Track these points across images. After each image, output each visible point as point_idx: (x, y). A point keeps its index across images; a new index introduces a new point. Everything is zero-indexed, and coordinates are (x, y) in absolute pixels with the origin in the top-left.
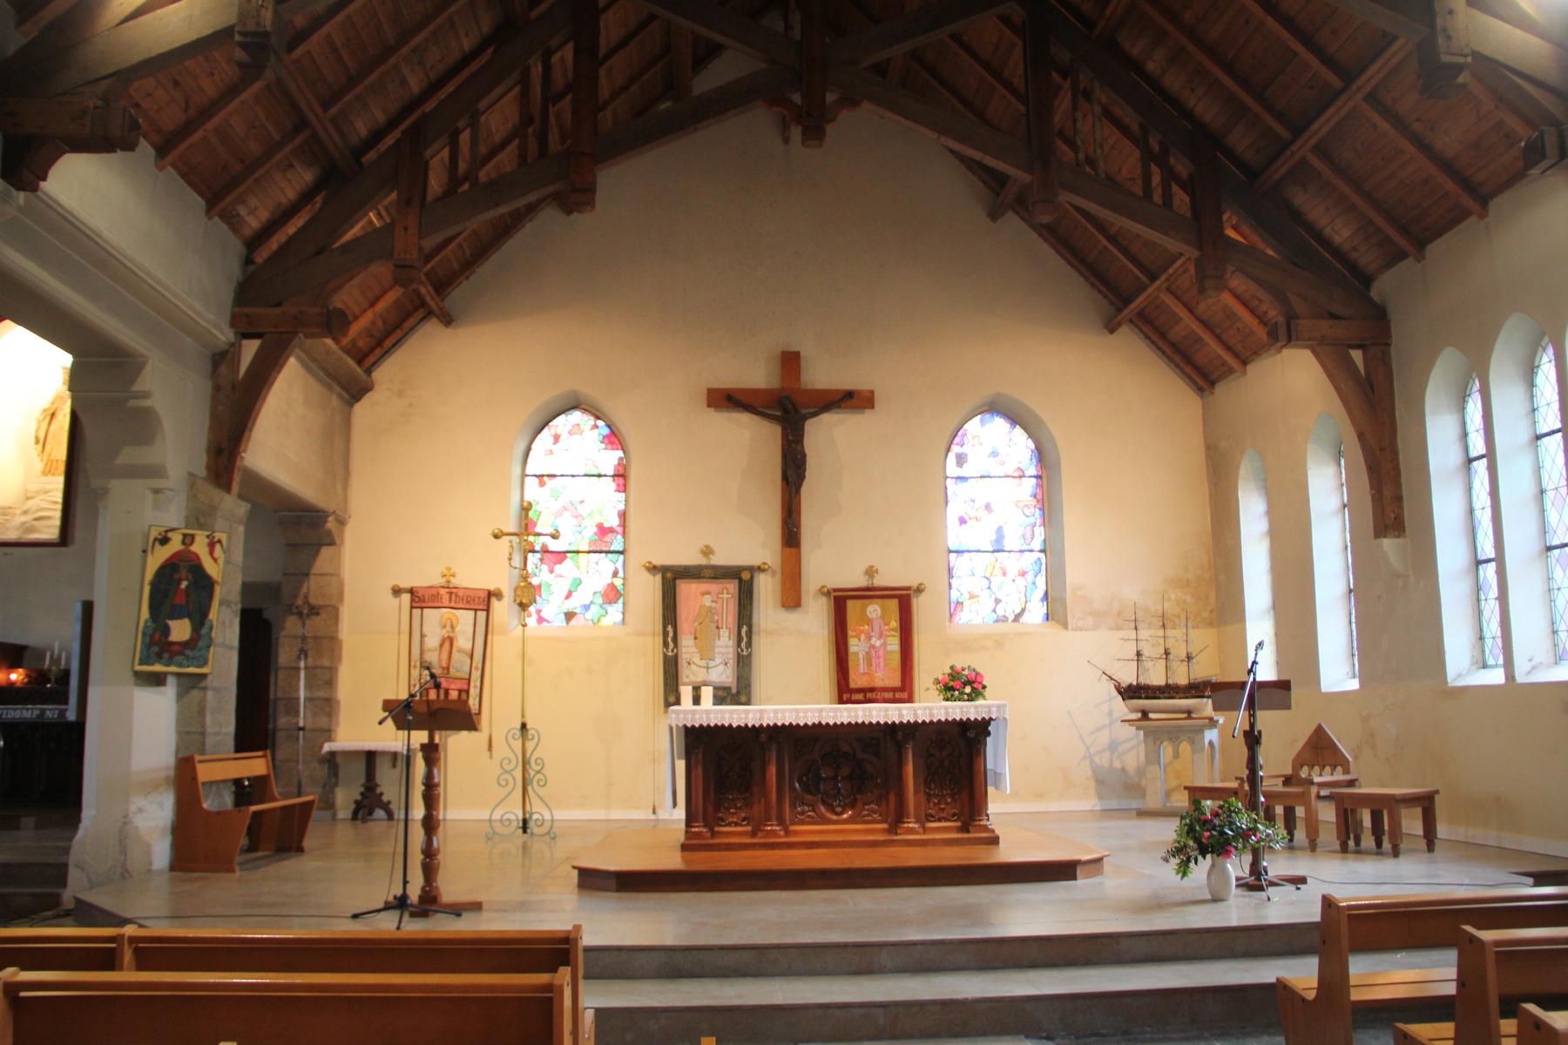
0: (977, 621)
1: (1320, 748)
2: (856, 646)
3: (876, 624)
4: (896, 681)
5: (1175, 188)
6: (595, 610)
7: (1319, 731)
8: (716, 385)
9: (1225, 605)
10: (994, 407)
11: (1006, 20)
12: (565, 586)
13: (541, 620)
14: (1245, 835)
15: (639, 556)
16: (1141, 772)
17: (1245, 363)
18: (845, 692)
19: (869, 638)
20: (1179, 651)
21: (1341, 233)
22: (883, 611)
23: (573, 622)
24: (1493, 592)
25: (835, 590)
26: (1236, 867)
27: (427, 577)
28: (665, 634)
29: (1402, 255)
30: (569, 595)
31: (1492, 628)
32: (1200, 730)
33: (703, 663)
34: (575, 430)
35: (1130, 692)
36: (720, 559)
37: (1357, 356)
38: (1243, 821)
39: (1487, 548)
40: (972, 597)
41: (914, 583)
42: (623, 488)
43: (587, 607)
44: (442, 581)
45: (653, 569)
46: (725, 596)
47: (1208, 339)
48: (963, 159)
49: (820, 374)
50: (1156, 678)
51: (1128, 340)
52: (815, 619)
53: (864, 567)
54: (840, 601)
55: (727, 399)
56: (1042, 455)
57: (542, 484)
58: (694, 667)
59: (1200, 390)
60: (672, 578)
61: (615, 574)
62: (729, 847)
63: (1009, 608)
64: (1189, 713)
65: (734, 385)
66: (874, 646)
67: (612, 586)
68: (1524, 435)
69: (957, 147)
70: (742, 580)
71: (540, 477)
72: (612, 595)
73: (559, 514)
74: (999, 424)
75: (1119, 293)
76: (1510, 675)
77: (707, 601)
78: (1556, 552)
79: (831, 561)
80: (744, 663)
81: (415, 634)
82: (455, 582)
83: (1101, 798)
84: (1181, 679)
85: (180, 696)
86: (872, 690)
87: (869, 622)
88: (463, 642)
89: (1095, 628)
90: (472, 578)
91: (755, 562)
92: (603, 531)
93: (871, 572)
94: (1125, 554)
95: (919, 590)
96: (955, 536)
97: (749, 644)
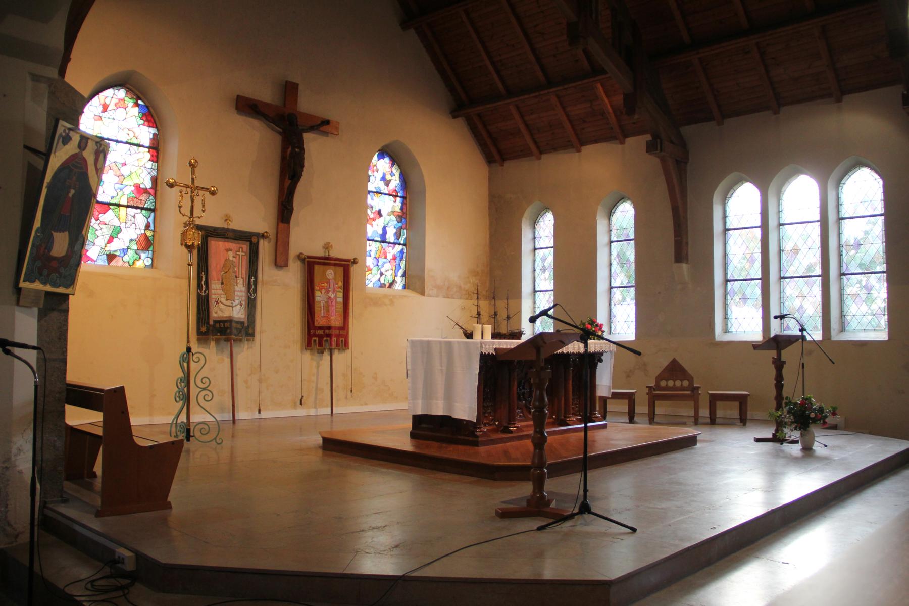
2: (319, 297)
3: (332, 283)
6: (131, 253)
8: (241, 94)
12: (106, 232)
17: (541, 153)
19: (328, 292)
22: (335, 274)
23: (113, 263)
24: (204, 280)
25: (309, 257)
30: (110, 240)
33: (229, 303)
34: (120, 104)
36: (235, 225)
41: (350, 257)
42: (155, 158)
43: (125, 251)
46: (241, 253)
51: (460, 122)
52: (293, 277)
53: (322, 244)
54: (311, 266)
55: (247, 106)
58: (221, 305)
59: (490, 160)
61: (147, 227)
63: (388, 277)
65: (250, 97)
67: (147, 238)
72: (146, 244)
77: (230, 255)
78: (787, 280)
80: (251, 304)
85: (42, 315)
87: (328, 282)
89: (437, 296)
92: (139, 190)
93: (327, 247)
95: (355, 262)
97: (255, 291)
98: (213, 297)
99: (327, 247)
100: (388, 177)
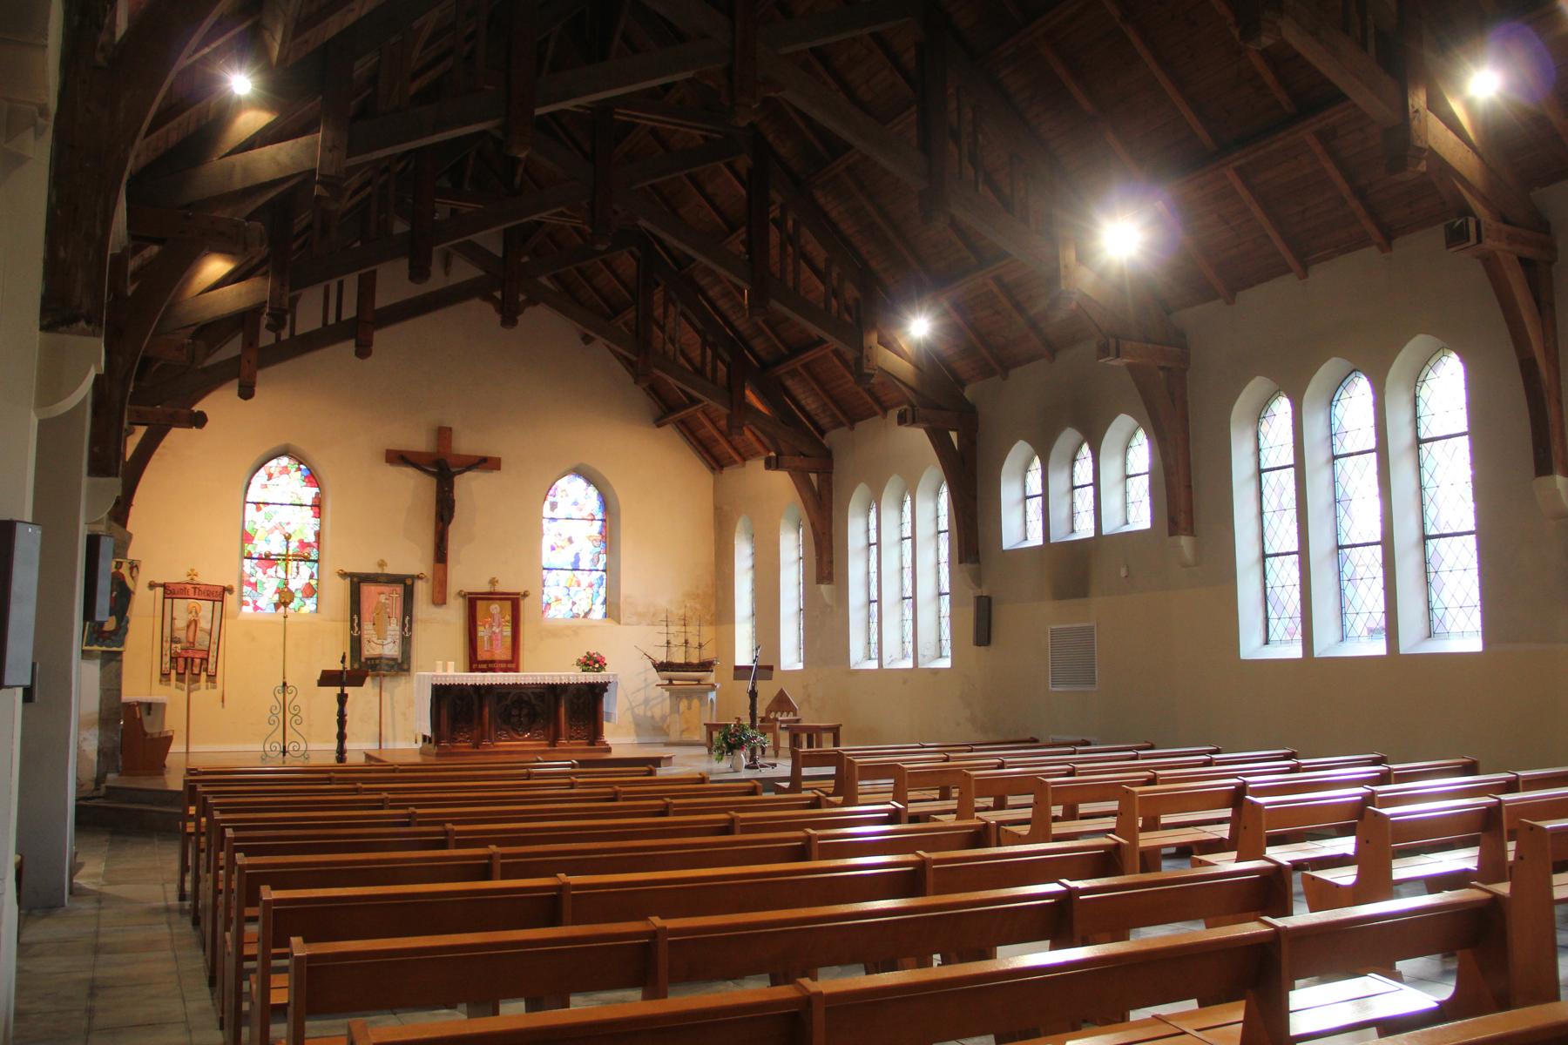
0: (560, 616)
1: (782, 702)
2: (482, 632)
4: (507, 656)
5: (720, 364)
7: (782, 692)
9: (722, 612)
10: (591, 478)
11: (631, 253)
13: (256, 608)
14: (749, 740)
15: (332, 565)
16: (664, 718)
17: (744, 460)
18: (474, 663)
20: (694, 642)
21: (811, 404)
26: (743, 757)
27: (177, 576)
28: (352, 621)
29: (841, 424)
31: (874, 638)
32: (706, 692)
34: (285, 471)
35: (661, 667)
36: (389, 570)
37: (813, 477)
38: (750, 733)
39: (874, 596)
40: (558, 600)
41: (521, 590)
44: (188, 579)
45: (344, 575)
47: (722, 440)
48: (613, 351)
49: (466, 443)
50: (679, 658)
51: (669, 433)
52: (454, 613)
54: (472, 602)
55: (398, 458)
56: (606, 503)
57: (259, 509)
60: (357, 582)
61: (312, 577)
62: (463, 754)
63: (581, 608)
64: (699, 680)
65: (403, 448)
66: (493, 633)
68: (896, 537)
69: (613, 346)
70: (406, 584)
71: (256, 503)
73: (271, 532)
74: (580, 483)
75: (667, 410)
76: (880, 665)
77: (382, 598)
79: (466, 574)
80: (406, 642)
81: (167, 618)
82: (200, 579)
83: (638, 735)
84: (695, 661)
85: (102, 666)
86: (492, 662)
87: (492, 616)
88: (204, 624)
90: (211, 576)
91: (416, 572)
93: (493, 582)
94: (659, 577)
95: (525, 595)
96: (548, 558)
97: (410, 629)
98: (365, 637)
99: (493, 582)
100: (581, 501)
